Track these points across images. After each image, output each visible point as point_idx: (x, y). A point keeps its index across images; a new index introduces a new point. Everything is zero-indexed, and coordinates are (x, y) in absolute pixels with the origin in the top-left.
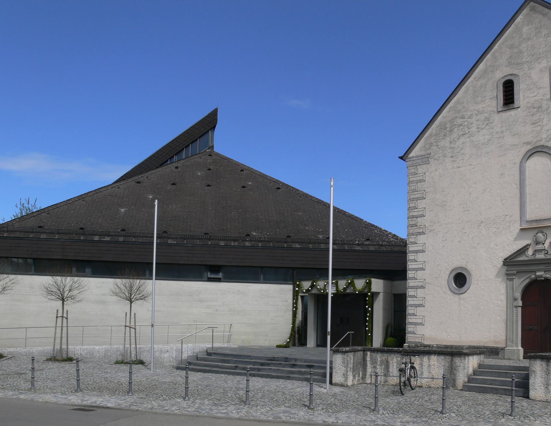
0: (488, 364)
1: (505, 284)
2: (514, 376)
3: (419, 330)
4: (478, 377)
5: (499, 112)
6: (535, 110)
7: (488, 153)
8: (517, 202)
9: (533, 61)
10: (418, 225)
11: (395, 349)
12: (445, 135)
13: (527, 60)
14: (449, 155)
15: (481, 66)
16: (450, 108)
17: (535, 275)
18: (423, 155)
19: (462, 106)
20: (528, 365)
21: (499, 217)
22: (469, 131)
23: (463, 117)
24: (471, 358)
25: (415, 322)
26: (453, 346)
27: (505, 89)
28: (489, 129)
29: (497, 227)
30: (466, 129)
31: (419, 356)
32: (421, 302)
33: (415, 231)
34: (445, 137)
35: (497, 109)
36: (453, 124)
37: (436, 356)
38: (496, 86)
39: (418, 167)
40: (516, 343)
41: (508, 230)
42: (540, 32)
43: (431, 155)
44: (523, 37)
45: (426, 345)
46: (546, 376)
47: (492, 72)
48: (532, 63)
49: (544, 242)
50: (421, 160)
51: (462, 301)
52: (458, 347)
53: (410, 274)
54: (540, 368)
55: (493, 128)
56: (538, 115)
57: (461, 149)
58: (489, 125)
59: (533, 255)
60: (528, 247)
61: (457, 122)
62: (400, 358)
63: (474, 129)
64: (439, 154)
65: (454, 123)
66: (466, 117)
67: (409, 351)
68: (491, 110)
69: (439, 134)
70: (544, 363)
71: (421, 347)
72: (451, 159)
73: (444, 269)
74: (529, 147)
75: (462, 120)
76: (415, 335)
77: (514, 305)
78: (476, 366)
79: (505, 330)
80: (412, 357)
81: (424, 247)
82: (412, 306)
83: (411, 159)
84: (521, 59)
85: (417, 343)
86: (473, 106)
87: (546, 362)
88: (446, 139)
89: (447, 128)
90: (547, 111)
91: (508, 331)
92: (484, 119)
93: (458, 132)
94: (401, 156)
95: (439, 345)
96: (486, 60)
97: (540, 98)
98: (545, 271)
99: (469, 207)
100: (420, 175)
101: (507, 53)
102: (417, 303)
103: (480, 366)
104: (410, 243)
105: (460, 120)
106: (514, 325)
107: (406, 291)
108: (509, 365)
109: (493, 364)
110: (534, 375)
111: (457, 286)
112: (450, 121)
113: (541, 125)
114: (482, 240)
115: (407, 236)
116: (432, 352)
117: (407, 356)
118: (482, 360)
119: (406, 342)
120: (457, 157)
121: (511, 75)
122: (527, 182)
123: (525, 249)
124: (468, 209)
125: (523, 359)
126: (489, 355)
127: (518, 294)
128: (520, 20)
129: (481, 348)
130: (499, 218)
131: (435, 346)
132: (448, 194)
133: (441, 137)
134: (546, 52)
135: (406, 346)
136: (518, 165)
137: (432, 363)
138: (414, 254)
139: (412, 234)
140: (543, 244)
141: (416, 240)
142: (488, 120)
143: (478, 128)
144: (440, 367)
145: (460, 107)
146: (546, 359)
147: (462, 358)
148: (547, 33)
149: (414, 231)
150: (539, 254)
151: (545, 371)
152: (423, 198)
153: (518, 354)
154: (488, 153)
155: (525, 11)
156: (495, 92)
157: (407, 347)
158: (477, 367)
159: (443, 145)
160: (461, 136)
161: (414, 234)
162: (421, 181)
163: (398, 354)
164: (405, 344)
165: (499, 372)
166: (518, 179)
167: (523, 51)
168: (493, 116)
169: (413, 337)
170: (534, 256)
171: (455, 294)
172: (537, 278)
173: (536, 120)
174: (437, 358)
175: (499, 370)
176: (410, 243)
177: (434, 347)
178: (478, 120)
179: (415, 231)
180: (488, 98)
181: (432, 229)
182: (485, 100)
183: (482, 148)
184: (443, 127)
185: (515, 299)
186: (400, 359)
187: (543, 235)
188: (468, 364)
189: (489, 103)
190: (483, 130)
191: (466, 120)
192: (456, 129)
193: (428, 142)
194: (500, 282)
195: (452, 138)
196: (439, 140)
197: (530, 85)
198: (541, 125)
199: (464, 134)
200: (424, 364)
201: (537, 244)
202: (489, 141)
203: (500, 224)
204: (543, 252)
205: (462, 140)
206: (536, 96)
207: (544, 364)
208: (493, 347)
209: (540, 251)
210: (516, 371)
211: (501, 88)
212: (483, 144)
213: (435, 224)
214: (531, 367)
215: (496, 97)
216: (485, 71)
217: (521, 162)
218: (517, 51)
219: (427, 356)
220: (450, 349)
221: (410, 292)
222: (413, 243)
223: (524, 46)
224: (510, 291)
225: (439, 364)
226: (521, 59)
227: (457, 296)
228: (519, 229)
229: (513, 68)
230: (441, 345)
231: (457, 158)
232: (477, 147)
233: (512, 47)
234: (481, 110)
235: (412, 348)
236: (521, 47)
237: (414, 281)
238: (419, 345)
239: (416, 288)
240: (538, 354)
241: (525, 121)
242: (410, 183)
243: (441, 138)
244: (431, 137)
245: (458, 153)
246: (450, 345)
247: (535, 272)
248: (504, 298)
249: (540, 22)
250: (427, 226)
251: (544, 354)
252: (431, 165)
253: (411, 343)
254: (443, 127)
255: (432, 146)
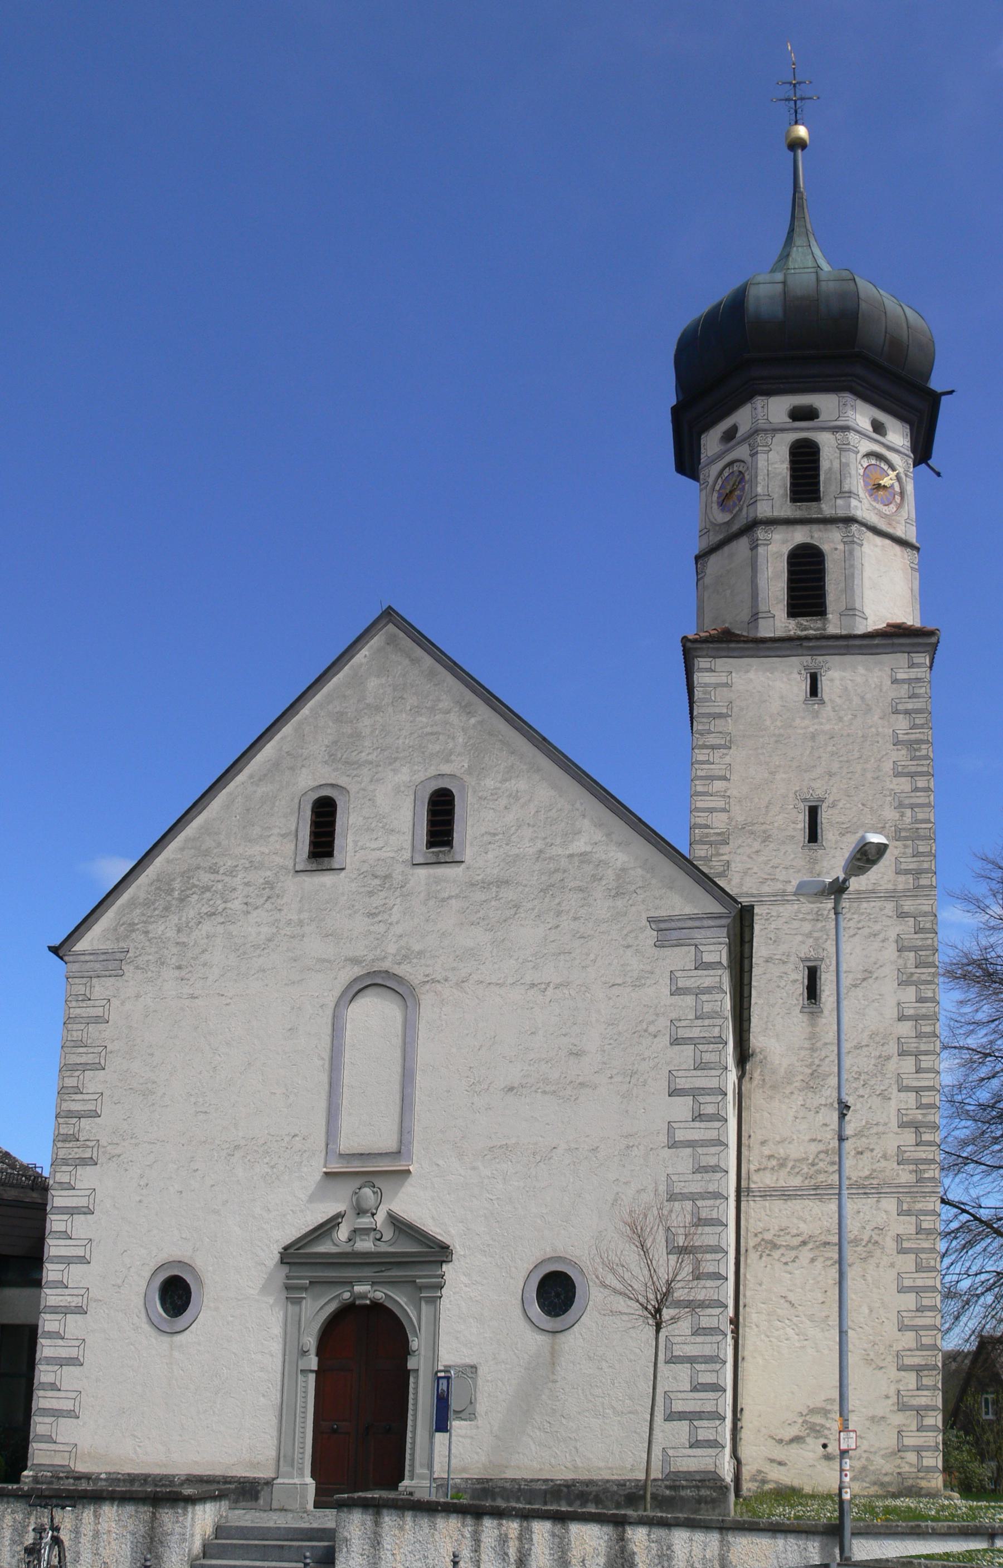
0: (237, 1524)
1: (281, 1313)
2: (308, 1554)
3: (66, 1431)
4: (214, 1562)
5: (297, 872)
6: (377, 882)
7: (264, 971)
8: (322, 1104)
9: (381, 763)
10: (81, 1139)
11: (10, 1487)
12: (166, 909)
13: (370, 757)
14: (173, 961)
15: (268, 751)
16: (187, 840)
17: (352, 1292)
18: (110, 951)
19: (214, 841)
20: (331, 1525)
21: (278, 1139)
22: (225, 908)
23: (214, 870)
24: (199, 1508)
25: (55, 1407)
26: (149, 1475)
27: (316, 818)
28: (271, 910)
29: (273, 1163)
30: (219, 902)
31: (74, 1506)
32: (73, 1353)
33: (73, 1153)
34: (167, 914)
35: (295, 865)
36: (188, 882)
37: (115, 1507)
38: (297, 806)
39: (94, 980)
40: (300, 1466)
41: (297, 1174)
42: (402, 698)
43: (129, 955)
44: (367, 702)
45: (81, 1475)
46: (372, 1550)
47: (292, 769)
48: (380, 769)
49: (375, 1211)
50: (103, 963)
51: (176, 1354)
52: (161, 1480)
53: (51, 1272)
54: (360, 1530)
55: (280, 910)
56: (382, 894)
57: (203, 952)
58: (273, 900)
59: (350, 1240)
60: (340, 1220)
61: (199, 880)
62: (23, 1513)
63: (236, 905)
64: (149, 954)
65: (191, 881)
66: (221, 871)
67: (47, 1493)
68: (281, 864)
69: (153, 903)
70: (369, 1518)
71: (67, 1482)
72: (177, 973)
73: (138, 1263)
74: (357, 971)
75: (212, 877)
76: (53, 1447)
77: (300, 1368)
78: (209, 1530)
79: (275, 1434)
80: (58, 1514)
81: (91, 1201)
82: (50, 1361)
83: (80, 957)
84: (356, 752)
85: (57, 1468)
86: (239, 845)
87: (374, 1515)
88: (170, 920)
89: (173, 890)
90: (403, 889)
91: (283, 1435)
92: (263, 884)
93: (200, 905)
94: (53, 945)
95: (114, 1473)
96: (282, 738)
97: (392, 855)
98: (373, 1284)
99: (210, 1105)
100: (97, 1003)
101: (329, 731)
102: (64, 1353)
103: (219, 1531)
104: (56, 1186)
105: (207, 875)
106: (298, 1419)
107: (38, 1319)
108: (287, 1526)
109: (249, 1524)
110: (345, 1550)
111: (165, 1312)
112: (184, 872)
113: (387, 920)
114: (234, 1194)
115: (52, 1165)
116: (105, 1494)
117: (45, 1507)
118: (224, 1514)
119: (29, 1464)
120: (190, 969)
121: (333, 785)
122: (348, 1057)
123: (331, 1224)
124: (206, 1109)
125: (315, 1508)
126: (236, 1501)
127: (310, 1339)
128: (364, 661)
129: (218, 1482)
130: (276, 1141)
131: (103, 1476)
132: (163, 1063)
133: (157, 912)
134: (411, 749)
135: (28, 1477)
136: (329, 1012)
137: (104, 1526)
138: (65, 1217)
139: (65, 1162)
140: (373, 1215)
141: (73, 1178)
142: (272, 888)
143: (246, 904)
144: (123, 1536)
145: (209, 842)
146: (375, 1506)
147: (180, 1511)
148: (416, 704)
149: (70, 1154)
150: (362, 1240)
151: (369, 1538)
152: (98, 1066)
153: (304, 1497)
154: (264, 971)
155: (376, 641)
156: (293, 820)
157: (31, 1479)
158: (213, 1533)
159: (160, 933)
160: (205, 916)
161: (70, 1162)
162: (99, 1020)
163: (17, 1502)
164: (25, 1473)
165: (265, 1546)
166: (328, 1046)
167: (363, 734)
168: (282, 878)
169: (48, 1453)
170: (351, 1243)
171: (160, 1333)
172: (354, 1299)
173: (376, 908)
174: (117, 1512)
175: (263, 1540)
176: (56, 1186)
177: (101, 1479)
178: (247, 884)
179: (73, 1153)
180: (276, 831)
181: (117, 1152)
182: (269, 836)
183: (250, 956)
184: (163, 885)
185: (304, 1353)
186: (21, 1516)
187: (374, 1193)
188: (192, 1526)
189: (278, 847)
190: (257, 911)
191: (219, 877)
192: (194, 896)
193: (124, 919)
194: (271, 1306)
195: (184, 919)
196: (152, 920)
197: (370, 820)
198: (387, 920)
199: (214, 914)
200: (83, 1530)
201: (359, 1214)
202: (270, 940)
203: (280, 1157)
204: (372, 1234)
205: (207, 927)
206: (381, 849)
207: (369, 1519)
208: (246, 1479)
209: (365, 1231)
210: (302, 1540)
211: (308, 814)
212: (255, 947)
213: (124, 1140)
214: (341, 1530)
215: (294, 832)
216: (276, 765)
217: (337, 1005)
218: (350, 731)
219: (92, 1508)
220: (142, 1485)
221: (48, 1323)
222: (66, 1186)
223: (366, 723)
224: (292, 1329)
225: (121, 1529)
226: (356, 752)
227: (166, 1339)
228: (321, 1174)
229: (336, 770)
230: (119, 1473)
231: (190, 972)
232: (241, 951)
233: (339, 718)
234: (258, 858)
235: (42, 1483)
236: (361, 724)
237: (59, 1291)
238: (61, 1475)
239: (65, 1311)
240: (356, 1495)
241: (353, 906)
242: (71, 1021)
243: (157, 915)
244: (133, 906)
245: (194, 959)
246: (142, 1474)
247: (350, 1283)
248: (276, 1347)
249: (404, 675)
250: (103, 1142)
251: (369, 1495)
252: (127, 981)
253: (43, 1468)
254: (163, 885)
255: (133, 931)
